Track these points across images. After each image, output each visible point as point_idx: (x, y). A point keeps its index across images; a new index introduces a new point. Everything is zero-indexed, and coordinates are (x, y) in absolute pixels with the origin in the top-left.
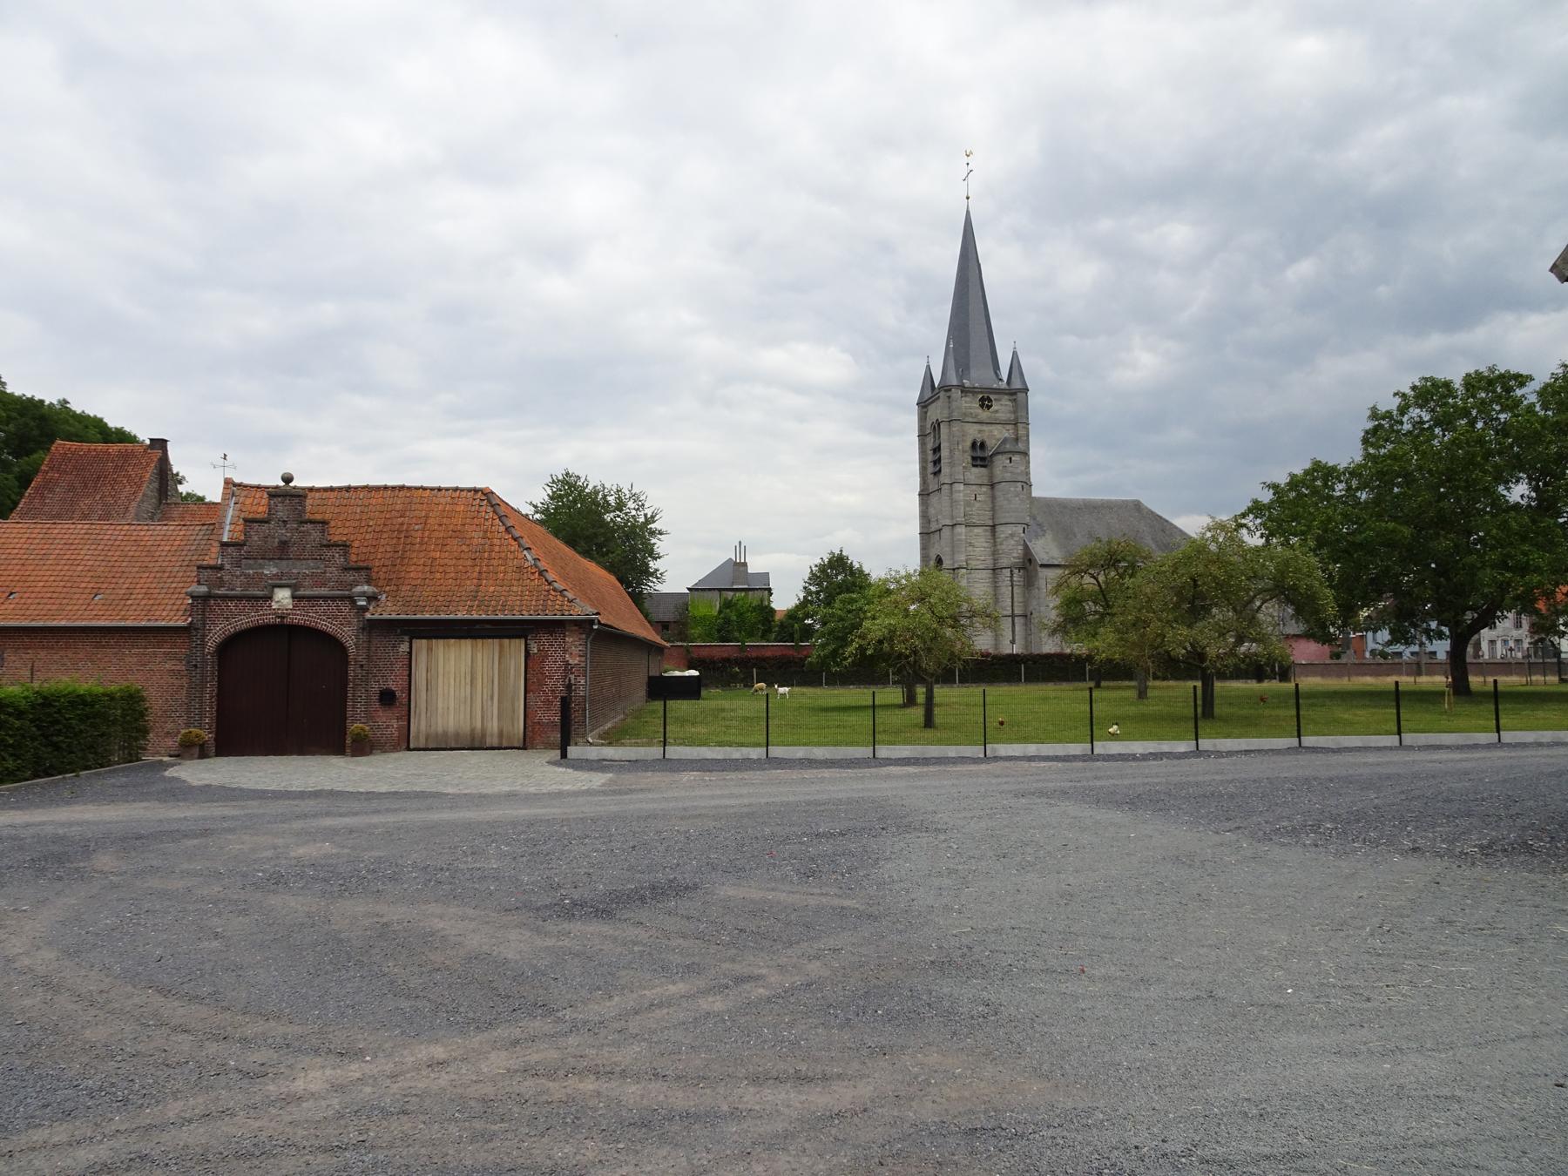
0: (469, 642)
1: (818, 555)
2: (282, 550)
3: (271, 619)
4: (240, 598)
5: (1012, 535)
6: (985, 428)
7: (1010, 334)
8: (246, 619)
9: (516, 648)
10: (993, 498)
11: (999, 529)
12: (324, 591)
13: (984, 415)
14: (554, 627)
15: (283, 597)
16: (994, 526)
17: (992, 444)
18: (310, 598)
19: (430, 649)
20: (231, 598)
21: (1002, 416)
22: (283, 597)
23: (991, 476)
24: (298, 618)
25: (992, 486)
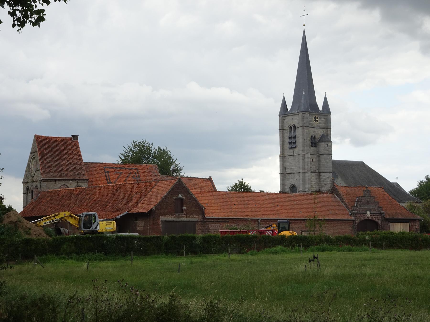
0: (399, 224)
1: (24, 151)
2: (368, 203)
3: (366, 218)
4: (361, 213)
5: (328, 177)
6: (316, 130)
7: (321, 91)
8: (362, 218)
9: (407, 224)
10: (319, 161)
11: (322, 174)
12: (375, 212)
13: (316, 124)
14: (414, 220)
15: (368, 213)
16: (319, 173)
17: (318, 137)
18: (373, 214)
19: (393, 225)
20: (359, 213)
21: (322, 125)
22: (368, 213)
23: (318, 151)
24: (371, 218)
25: (319, 155)
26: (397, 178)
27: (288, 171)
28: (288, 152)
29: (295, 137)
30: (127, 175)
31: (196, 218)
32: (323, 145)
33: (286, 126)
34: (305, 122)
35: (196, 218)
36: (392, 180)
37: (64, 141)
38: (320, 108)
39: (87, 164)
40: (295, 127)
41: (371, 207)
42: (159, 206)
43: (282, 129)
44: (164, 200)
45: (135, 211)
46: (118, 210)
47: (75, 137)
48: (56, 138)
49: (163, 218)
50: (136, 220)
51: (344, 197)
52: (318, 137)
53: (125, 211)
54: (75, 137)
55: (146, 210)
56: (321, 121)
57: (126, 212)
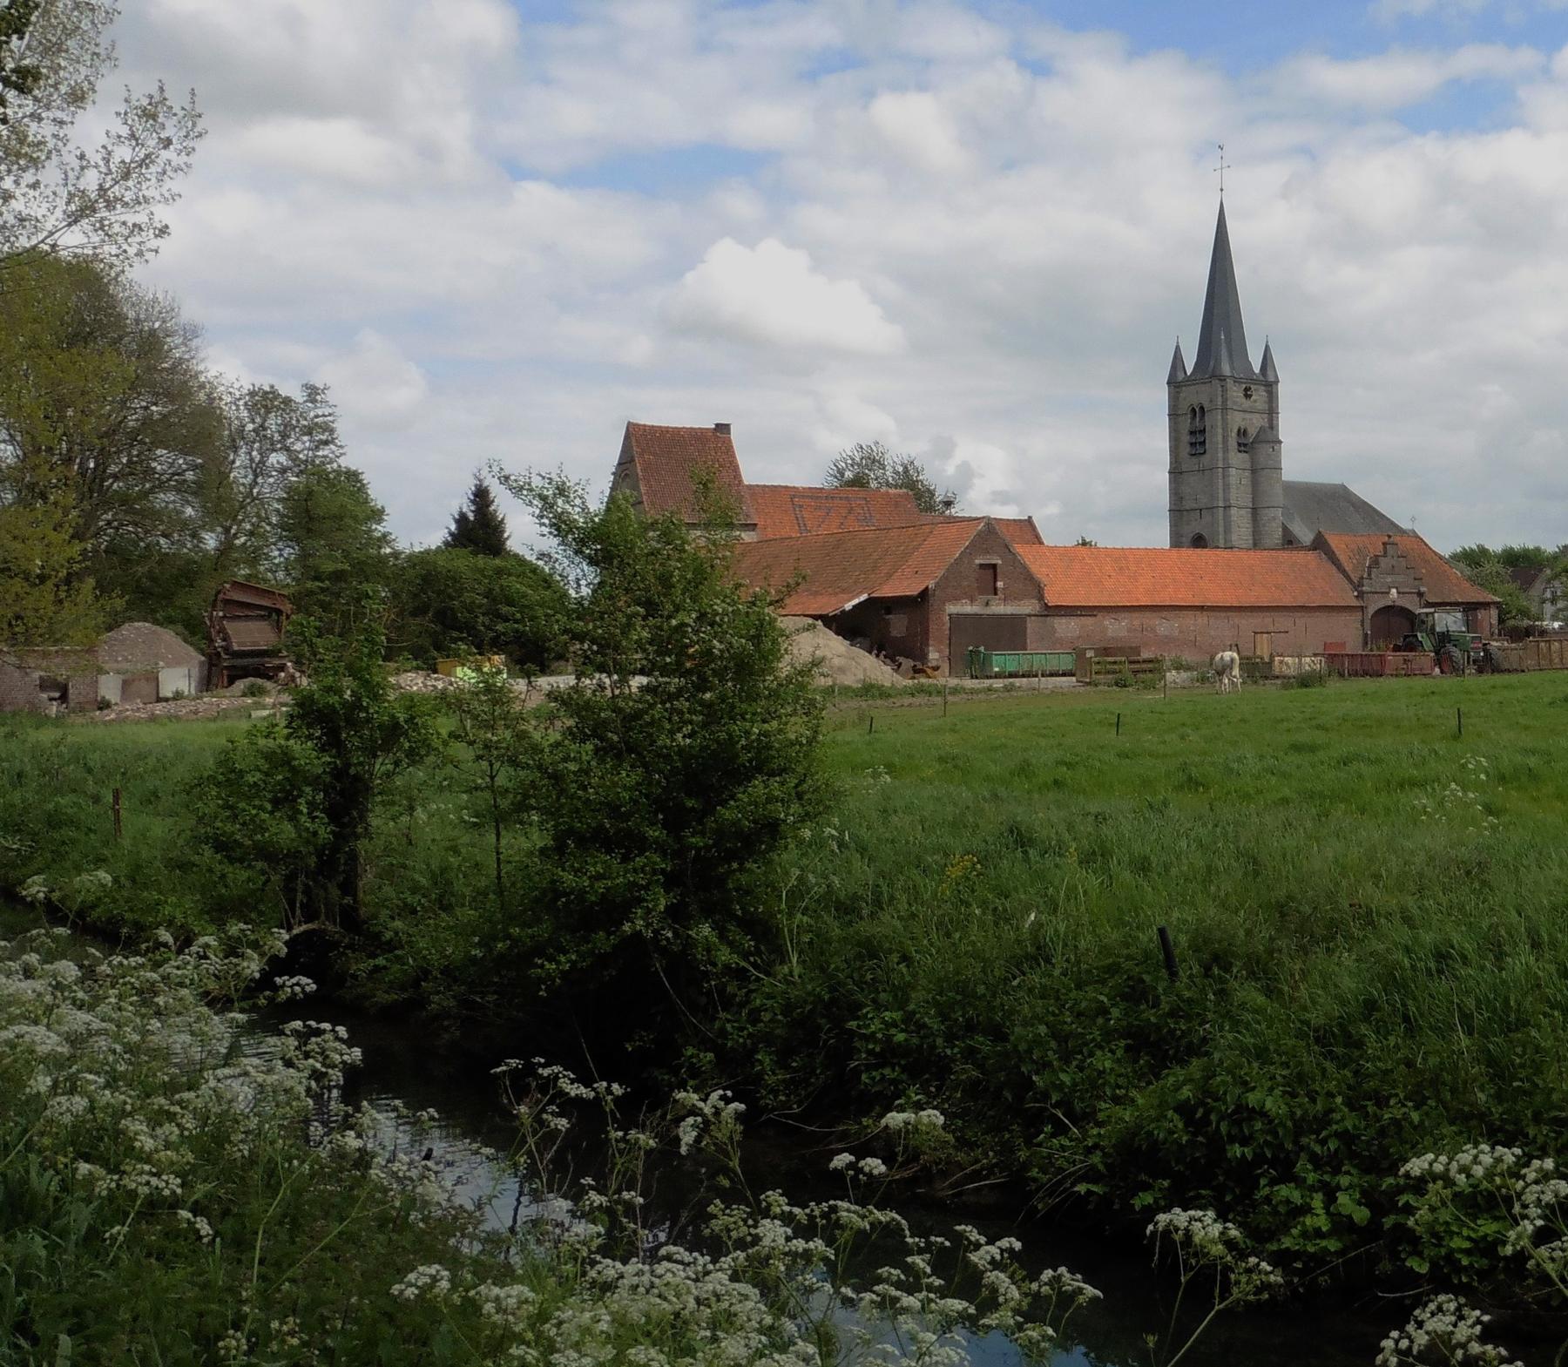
6: (1248, 416)
8: (1382, 603)
13: (1246, 404)
26: (1413, 519)
27: (1188, 504)
28: (1188, 464)
29: (1203, 431)
30: (844, 512)
31: (1027, 607)
32: (1265, 449)
33: (1184, 408)
34: (1217, 400)
35: (1027, 607)
36: (1405, 525)
37: (696, 437)
38: (1257, 370)
39: (750, 487)
40: (1202, 408)
41: (1400, 579)
42: (943, 582)
43: (1173, 415)
44: (954, 570)
45: (888, 591)
46: (843, 591)
47: (723, 428)
48: (677, 430)
49: (952, 609)
50: (889, 613)
51: (1342, 557)
52: (1252, 432)
53: (861, 593)
54: (723, 428)
55: (913, 590)
56: (1259, 395)
57: (864, 597)
